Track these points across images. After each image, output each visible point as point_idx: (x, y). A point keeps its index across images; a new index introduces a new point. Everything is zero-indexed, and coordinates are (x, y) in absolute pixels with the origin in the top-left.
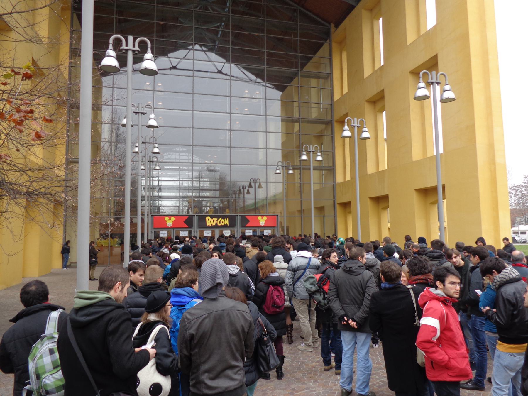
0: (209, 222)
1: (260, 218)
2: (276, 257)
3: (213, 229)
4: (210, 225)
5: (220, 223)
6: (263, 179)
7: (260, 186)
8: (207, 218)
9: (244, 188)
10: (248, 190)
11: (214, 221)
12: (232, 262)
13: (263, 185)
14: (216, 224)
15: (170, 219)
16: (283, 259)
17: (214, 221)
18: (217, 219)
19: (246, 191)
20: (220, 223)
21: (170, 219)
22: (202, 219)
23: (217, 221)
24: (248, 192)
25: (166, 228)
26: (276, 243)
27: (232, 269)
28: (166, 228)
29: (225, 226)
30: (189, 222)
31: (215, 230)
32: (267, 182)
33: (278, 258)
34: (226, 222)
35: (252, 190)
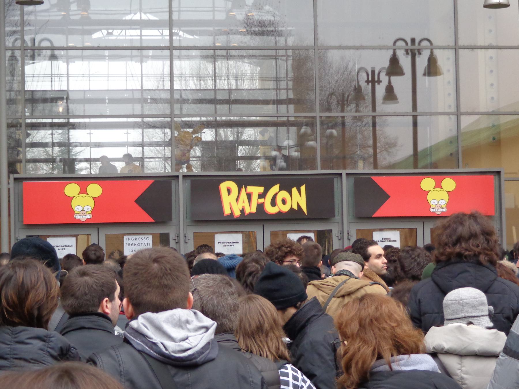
0: (233, 200)
1: (427, 183)
2: (453, 295)
3: (249, 228)
4: (237, 213)
5: (273, 203)
6: (441, 36)
7: (432, 69)
8: (224, 186)
9: (373, 81)
10: (390, 89)
11: (249, 196)
12: (177, 294)
13: (445, 59)
14: (260, 207)
15: (83, 191)
16: (486, 309)
17: (249, 196)
18: (261, 189)
19: (381, 90)
20: (273, 203)
21: (83, 191)
22: (205, 189)
23: (262, 196)
24: (390, 94)
25: (72, 226)
26: (459, 240)
27: (177, 333)
28: (72, 226)
29: (293, 217)
30: (155, 199)
31: (257, 229)
32: (456, 48)
33: (461, 304)
34: (298, 199)
35: (401, 84)
